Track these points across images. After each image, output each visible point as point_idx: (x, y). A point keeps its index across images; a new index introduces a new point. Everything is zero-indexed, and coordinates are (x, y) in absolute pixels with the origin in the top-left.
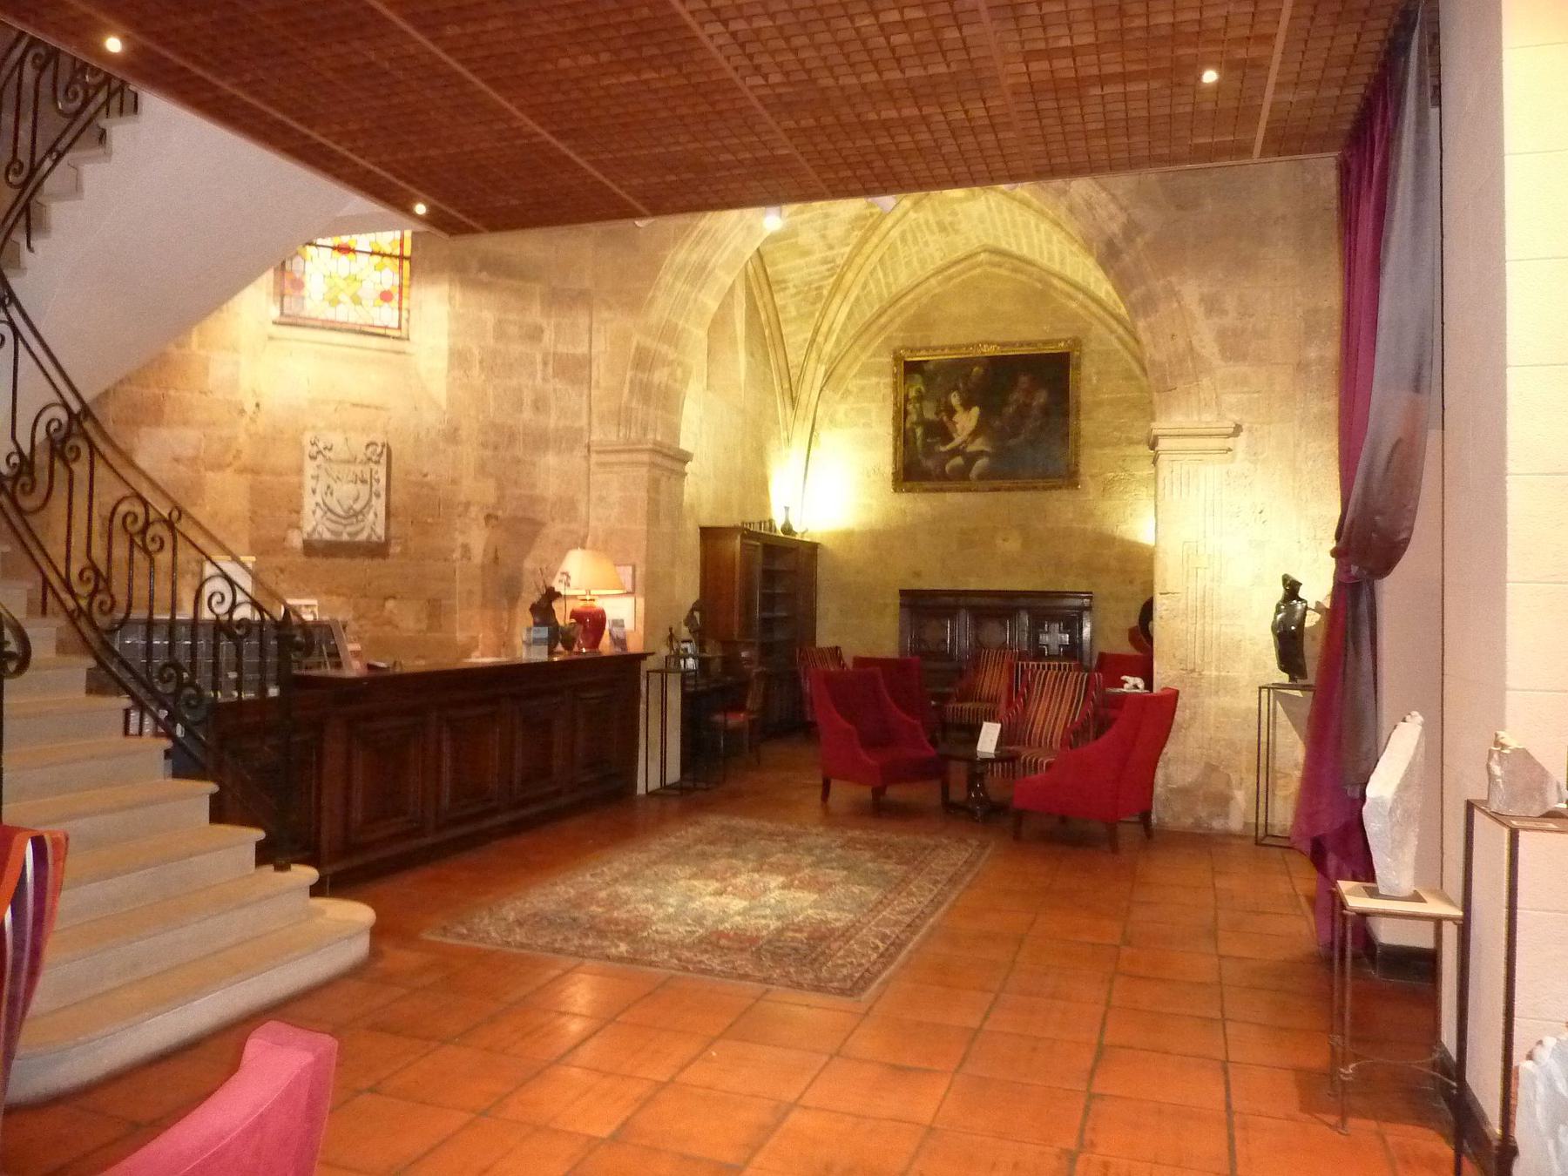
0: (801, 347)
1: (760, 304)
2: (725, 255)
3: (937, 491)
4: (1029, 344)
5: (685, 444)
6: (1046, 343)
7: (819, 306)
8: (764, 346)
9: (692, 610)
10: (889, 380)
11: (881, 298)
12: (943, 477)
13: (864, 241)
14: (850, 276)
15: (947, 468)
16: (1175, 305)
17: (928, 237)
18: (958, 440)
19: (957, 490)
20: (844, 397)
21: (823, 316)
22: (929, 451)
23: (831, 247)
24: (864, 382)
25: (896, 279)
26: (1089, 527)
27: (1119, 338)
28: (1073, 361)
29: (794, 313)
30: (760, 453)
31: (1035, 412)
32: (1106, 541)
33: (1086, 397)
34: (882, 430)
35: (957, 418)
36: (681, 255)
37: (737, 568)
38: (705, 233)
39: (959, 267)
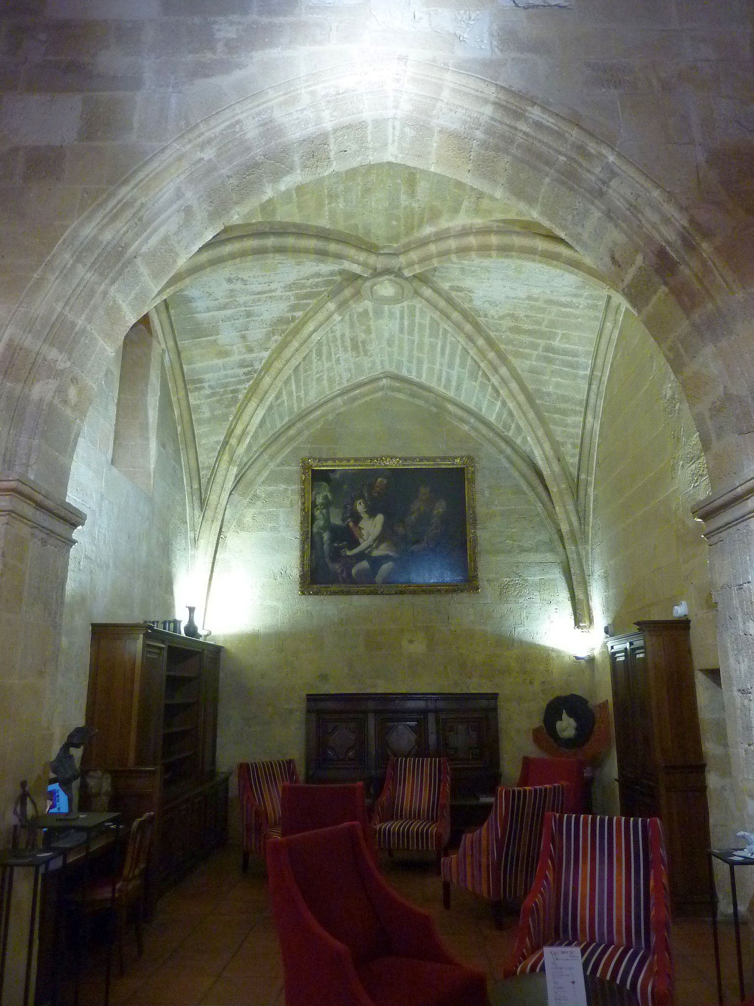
0: (214, 449)
1: (174, 399)
2: (153, 242)
3: (342, 593)
4: (428, 459)
5: (73, 497)
6: (443, 459)
7: (234, 410)
8: (175, 441)
9: (70, 743)
10: (296, 487)
11: (291, 411)
12: (350, 580)
14: (267, 380)
15: (354, 571)
17: (341, 354)
18: (363, 545)
19: (364, 593)
20: (251, 503)
21: (237, 418)
22: (336, 555)
23: (250, 350)
24: (271, 489)
25: (306, 394)
26: (489, 628)
27: (508, 458)
29: (207, 414)
30: (165, 552)
33: (481, 511)
34: (290, 533)
35: (362, 524)
36: (89, 230)
37: (137, 678)
38: (127, 205)
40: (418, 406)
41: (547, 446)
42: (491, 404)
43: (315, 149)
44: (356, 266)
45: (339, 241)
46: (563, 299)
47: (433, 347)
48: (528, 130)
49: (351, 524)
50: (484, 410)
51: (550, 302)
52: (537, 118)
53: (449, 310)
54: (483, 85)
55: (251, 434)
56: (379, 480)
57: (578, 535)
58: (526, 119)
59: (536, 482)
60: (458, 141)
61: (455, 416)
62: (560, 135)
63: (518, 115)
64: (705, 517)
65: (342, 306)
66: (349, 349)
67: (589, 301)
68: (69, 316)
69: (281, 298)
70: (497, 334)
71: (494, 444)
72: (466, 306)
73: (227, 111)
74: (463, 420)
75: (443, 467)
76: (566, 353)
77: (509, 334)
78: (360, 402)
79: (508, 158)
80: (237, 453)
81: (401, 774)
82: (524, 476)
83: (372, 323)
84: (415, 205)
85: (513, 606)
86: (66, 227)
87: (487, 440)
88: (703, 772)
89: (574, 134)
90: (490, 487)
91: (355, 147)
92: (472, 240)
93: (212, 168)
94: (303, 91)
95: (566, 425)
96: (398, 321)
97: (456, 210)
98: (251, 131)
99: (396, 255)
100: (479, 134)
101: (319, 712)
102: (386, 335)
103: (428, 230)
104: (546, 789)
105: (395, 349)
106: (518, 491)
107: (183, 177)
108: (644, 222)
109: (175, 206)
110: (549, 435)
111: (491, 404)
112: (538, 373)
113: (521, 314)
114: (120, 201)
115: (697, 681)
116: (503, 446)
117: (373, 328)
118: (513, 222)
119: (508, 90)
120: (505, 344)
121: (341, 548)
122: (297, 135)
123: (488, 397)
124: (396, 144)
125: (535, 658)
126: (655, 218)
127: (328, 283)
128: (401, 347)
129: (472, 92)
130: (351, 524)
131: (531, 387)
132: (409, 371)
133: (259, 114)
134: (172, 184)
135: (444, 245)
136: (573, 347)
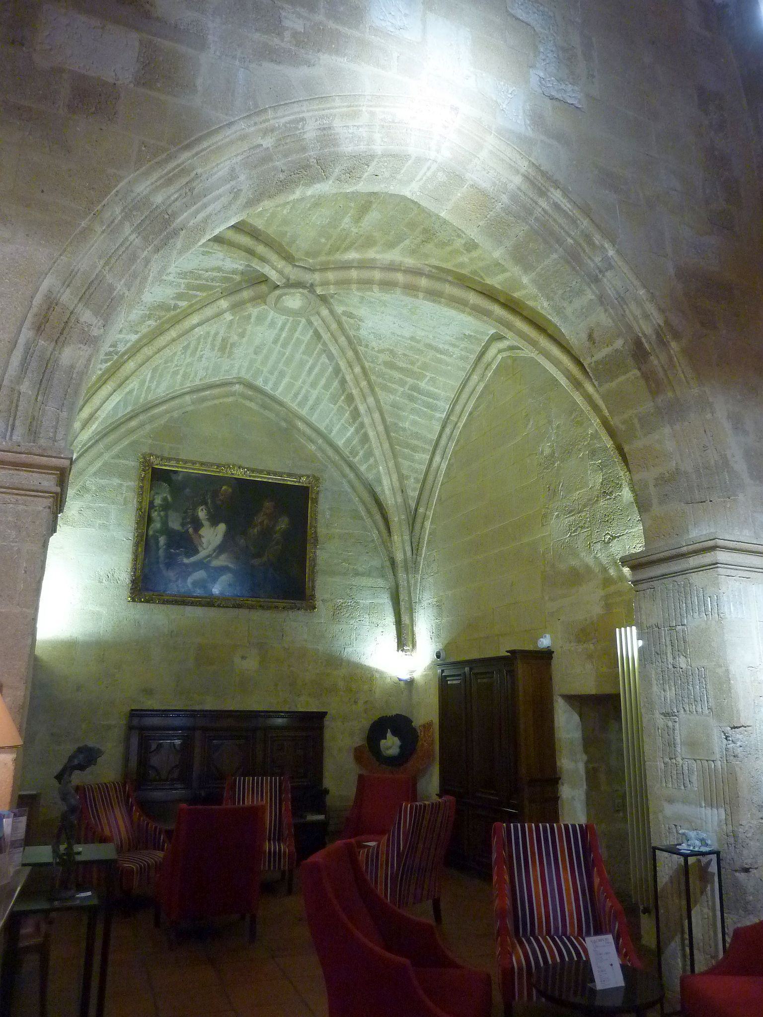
4: (275, 474)
6: (289, 475)
10: (133, 484)
13: (158, 332)
14: (131, 365)
16: (709, 416)
18: (202, 554)
24: (103, 482)
25: (157, 386)
26: (320, 648)
27: (349, 482)
28: (312, 495)
31: (277, 536)
32: (335, 661)
33: (322, 531)
35: (202, 532)
36: (142, 188)
38: (184, 172)
39: (216, 391)
40: (268, 418)
41: (395, 477)
42: (344, 429)
43: (358, 164)
44: (274, 272)
45: (266, 245)
46: (441, 346)
47: (302, 364)
48: (547, 208)
49: (191, 530)
50: (334, 432)
51: (429, 346)
52: (556, 200)
53: (338, 333)
54: (518, 157)
55: (100, 420)
56: (224, 488)
57: (410, 564)
58: (548, 198)
59: (375, 510)
60: (483, 199)
61: (304, 434)
62: (574, 221)
63: (542, 193)
64: (633, 568)
65: (236, 307)
66: (216, 348)
67: (463, 353)
68: (108, 277)
69: (171, 283)
70: (372, 365)
71: (337, 467)
72: (352, 333)
73: (295, 105)
74: (312, 441)
75: (289, 483)
76: (429, 394)
77: (382, 367)
78: (210, 403)
79: (527, 228)
80: (79, 439)
81: (239, 794)
82: (364, 503)
83: (249, 328)
84: (354, 230)
85: (344, 626)
86: (120, 179)
87: (332, 462)
88: (557, 783)
89: (585, 223)
90: (331, 509)
91: (387, 174)
92: (400, 277)
93: (267, 158)
94: (364, 109)
95: (413, 461)
96: (276, 331)
97: (391, 245)
98: (310, 133)
99: (312, 270)
100: (505, 198)
101: (142, 729)
102: (257, 342)
103: (352, 255)
104: (425, 806)
105: (260, 358)
106: (356, 516)
107: (240, 158)
108: (627, 312)
109: (228, 186)
110: (397, 466)
111: (344, 429)
112: (400, 409)
113: (400, 351)
114: (179, 165)
115: (556, 705)
116: (347, 470)
117: (248, 333)
118: (448, 272)
119: (538, 168)
120: (377, 377)
121: (179, 555)
122: (350, 149)
123: (342, 421)
124: (421, 183)
125: (360, 677)
126: (638, 312)
127: (226, 279)
128: (267, 358)
129: (508, 160)
130: (191, 530)
131: (389, 420)
132: (266, 382)
133: (322, 117)
134: (228, 162)
135: (366, 274)
136: (436, 390)
